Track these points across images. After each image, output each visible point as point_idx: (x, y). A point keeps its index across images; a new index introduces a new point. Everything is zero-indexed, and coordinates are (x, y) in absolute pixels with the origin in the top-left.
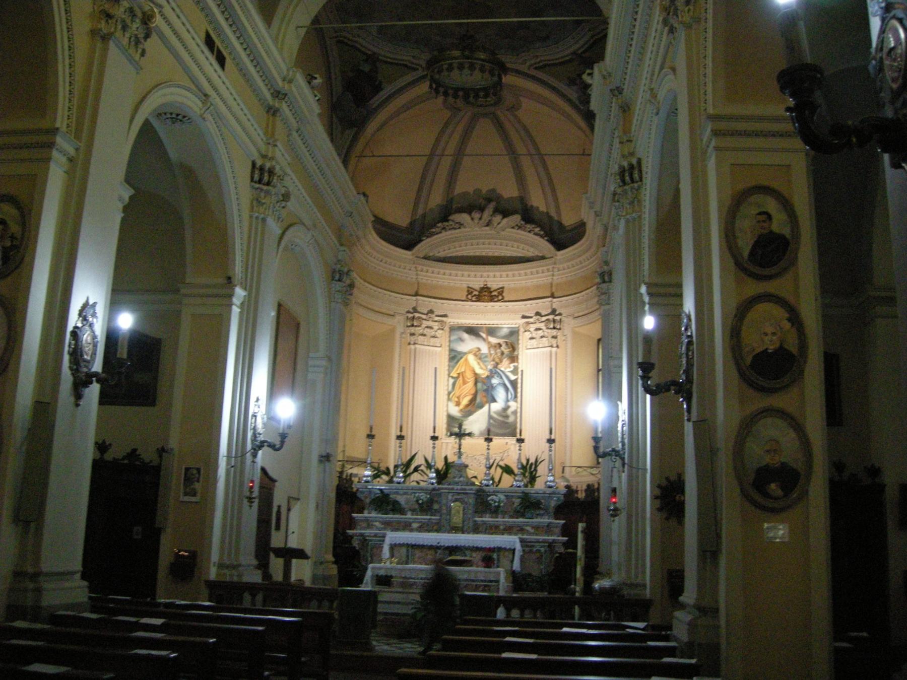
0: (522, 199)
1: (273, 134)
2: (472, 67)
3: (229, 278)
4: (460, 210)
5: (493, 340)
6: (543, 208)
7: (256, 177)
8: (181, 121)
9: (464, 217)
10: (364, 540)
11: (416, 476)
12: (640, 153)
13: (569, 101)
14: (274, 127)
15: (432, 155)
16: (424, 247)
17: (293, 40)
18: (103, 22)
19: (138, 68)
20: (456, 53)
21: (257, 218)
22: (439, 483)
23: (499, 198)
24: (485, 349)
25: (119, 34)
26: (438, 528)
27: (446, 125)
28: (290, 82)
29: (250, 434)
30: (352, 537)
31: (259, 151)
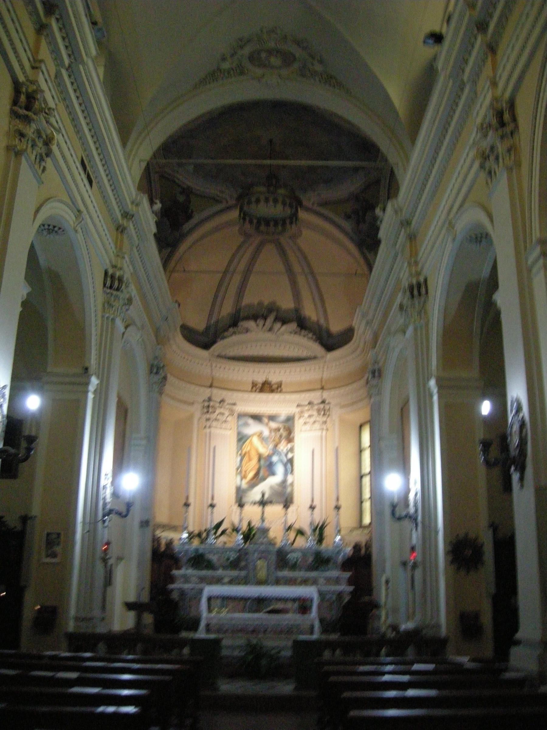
0: (297, 310)
1: (121, 249)
2: (276, 201)
3: (86, 369)
4: (247, 318)
5: (273, 425)
6: (314, 318)
7: (108, 283)
8: (56, 232)
9: (251, 324)
10: (182, 593)
11: (223, 539)
12: (426, 271)
13: (346, 234)
14: (122, 241)
15: (225, 273)
16: (217, 348)
17: (138, 170)
18: (17, 141)
19: (41, 182)
20: (262, 189)
21: (108, 318)
22: (245, 542)
23: (278, 310)
24: (266, 433)
25: (29, 150)
26: (245, 581)
27: (240, 247)
28: (137, 205)
29: (101, 503)
30: (172, 590)
31: (110, 262)
